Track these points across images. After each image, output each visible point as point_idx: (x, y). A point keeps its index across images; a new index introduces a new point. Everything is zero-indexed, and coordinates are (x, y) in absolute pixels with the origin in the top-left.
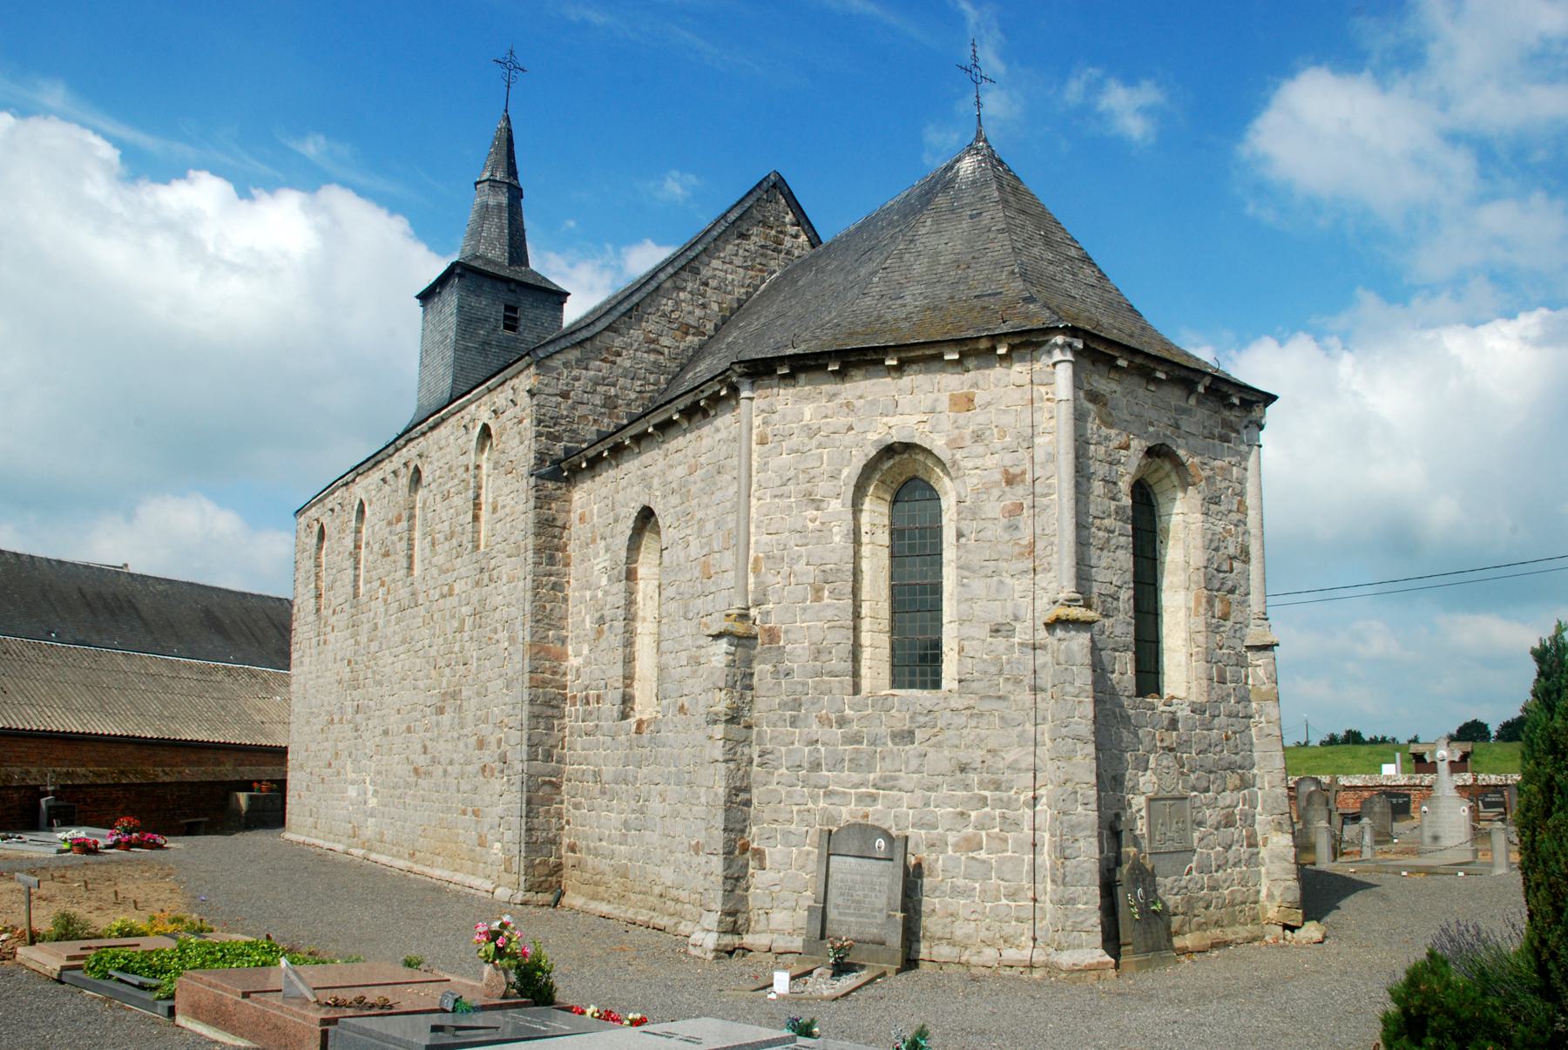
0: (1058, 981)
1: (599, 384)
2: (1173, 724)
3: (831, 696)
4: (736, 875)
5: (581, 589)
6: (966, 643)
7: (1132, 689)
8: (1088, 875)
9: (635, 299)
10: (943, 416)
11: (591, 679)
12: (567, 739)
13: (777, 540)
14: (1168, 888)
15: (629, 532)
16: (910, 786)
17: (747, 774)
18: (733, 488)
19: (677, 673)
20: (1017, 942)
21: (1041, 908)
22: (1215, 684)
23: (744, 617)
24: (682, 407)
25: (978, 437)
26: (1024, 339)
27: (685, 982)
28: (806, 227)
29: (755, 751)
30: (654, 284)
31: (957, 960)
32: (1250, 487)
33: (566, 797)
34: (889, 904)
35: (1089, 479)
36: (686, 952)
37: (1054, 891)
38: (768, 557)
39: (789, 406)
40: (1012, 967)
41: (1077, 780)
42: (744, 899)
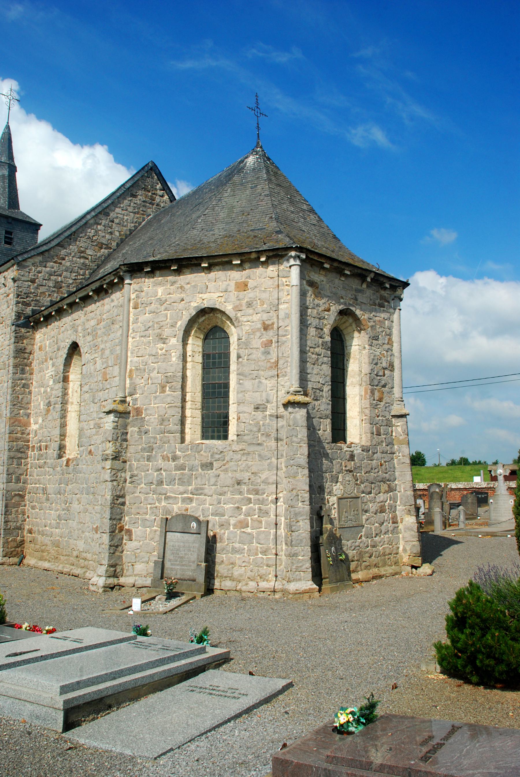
0: (288, 599)
1: (52, 275)
2: (352, 457)
3: (169, 445)
4: (116, 544)
5: (39, 387)
6: (241, 415)
7: (330, 439)
8: (304, 540)
9: (73, 229)
10: (231, 294)
11: (43, 436)
12: (29, 470)
13: (142, 360)
14: (349, 546)
15: (65, 356)
16: (210, 493)
17: (123, 488)
18: (120, 333)
19: (88, 433)
20: (267, 578)
21: (280, 559)
22: (375, 436)
23: (123, 402)
24: (94, 288)
25: (249, 305)
26: (275, 253)
27: (84, 606)
28: (168, 191)
29: (128, 475)
30: (84, 221)
31: (235, 589)
32: (395, 331)
33: (27, 502)
34: (198, 558)
35: (307, 327)
36: (88, 589)
37: (286, 549)
38: (137, 369)
39: (150, 288)
40: (264, 592)
41: (299, 489)
42: (121, 557)
